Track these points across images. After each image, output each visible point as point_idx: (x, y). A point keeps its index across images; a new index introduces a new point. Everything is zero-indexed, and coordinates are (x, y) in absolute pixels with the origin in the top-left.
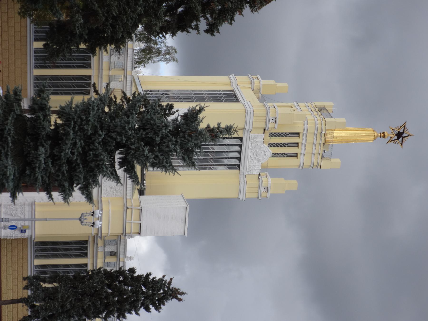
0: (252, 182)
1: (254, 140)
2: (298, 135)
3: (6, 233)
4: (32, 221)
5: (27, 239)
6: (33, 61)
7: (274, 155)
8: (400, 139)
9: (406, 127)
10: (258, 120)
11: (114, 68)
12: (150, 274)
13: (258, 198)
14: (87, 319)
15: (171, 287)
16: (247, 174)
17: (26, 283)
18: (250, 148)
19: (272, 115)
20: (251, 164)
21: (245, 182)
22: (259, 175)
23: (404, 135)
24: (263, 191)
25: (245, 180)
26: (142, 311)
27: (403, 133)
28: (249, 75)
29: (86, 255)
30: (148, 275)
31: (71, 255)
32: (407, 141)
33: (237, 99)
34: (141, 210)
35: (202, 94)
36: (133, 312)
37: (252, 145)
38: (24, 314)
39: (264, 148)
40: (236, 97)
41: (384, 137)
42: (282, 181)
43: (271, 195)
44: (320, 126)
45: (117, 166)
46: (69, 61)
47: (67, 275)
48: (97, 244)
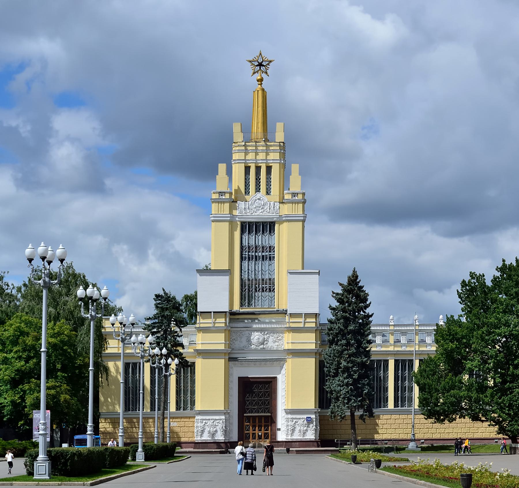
1: (243, 210)
2: (247, 169)
3: (221, 436)
8: (260, 61)
9: (251, 59)
10: (222, 209)
14: (371, 359)
16: (278, 215)
18: (252, 214)
20: (269, 211)
21: (285, 216)
24: (297, 198)
25: (284, 216)
32: (268, 56)
34: (290, 314)
36: (370, 319)
37: (249, 212)
39: (253, 200)
46: (159, 381)
47: (462, 361)
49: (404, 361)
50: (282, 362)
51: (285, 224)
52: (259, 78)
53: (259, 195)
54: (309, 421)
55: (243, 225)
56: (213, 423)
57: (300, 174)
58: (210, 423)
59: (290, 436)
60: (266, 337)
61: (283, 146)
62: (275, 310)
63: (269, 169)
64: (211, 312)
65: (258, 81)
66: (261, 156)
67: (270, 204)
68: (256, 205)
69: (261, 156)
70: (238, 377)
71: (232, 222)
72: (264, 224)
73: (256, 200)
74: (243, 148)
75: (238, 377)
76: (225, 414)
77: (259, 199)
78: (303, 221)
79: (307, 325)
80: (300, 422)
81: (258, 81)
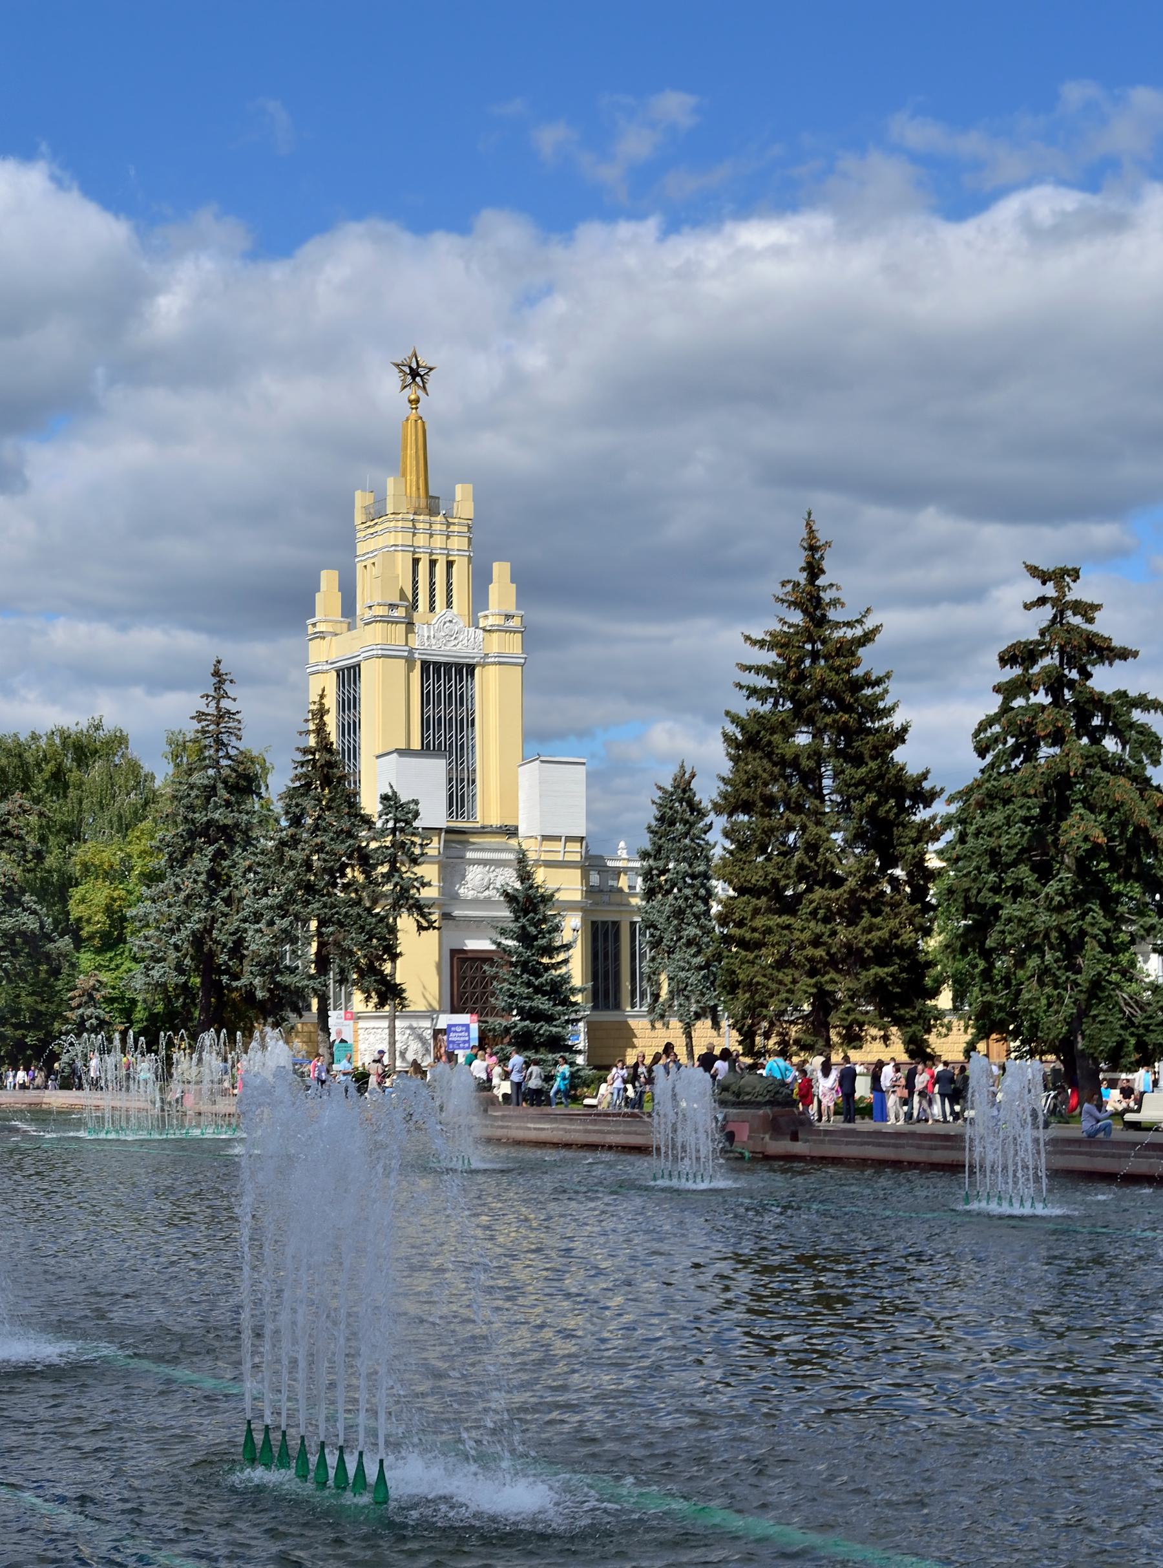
0: (495, 644)
7: (449, 604)
11: (102, 808)
13: (522, 665)
15: (671, 789)
17: (658, 1025)
19: (380, 611)
22: (485, 630)
23: (414, 366)
28: (470, 855)
29: (616, 925)
33: (354, 667)
35: (343, 725)
40: (349, 669)
41: (417, 401)
42: (493, 589)
43: (517, 608)
44: (400, 524)
45: (554, 961)
51: (492, 671)
52: (413, 397)
53: (450, 614)
55: (425, 665)
57: (512, 582)
59: (1028, 1204)
60: (492, 875)
62: (479, 825)
65: (410, 401)
66: (438, 541)
68: (447, 631)
69: (438, 541)
71: (410, 661)
72: (459, 667)
77: (451, 621)
79: (569, 857)
81: (410, 401)
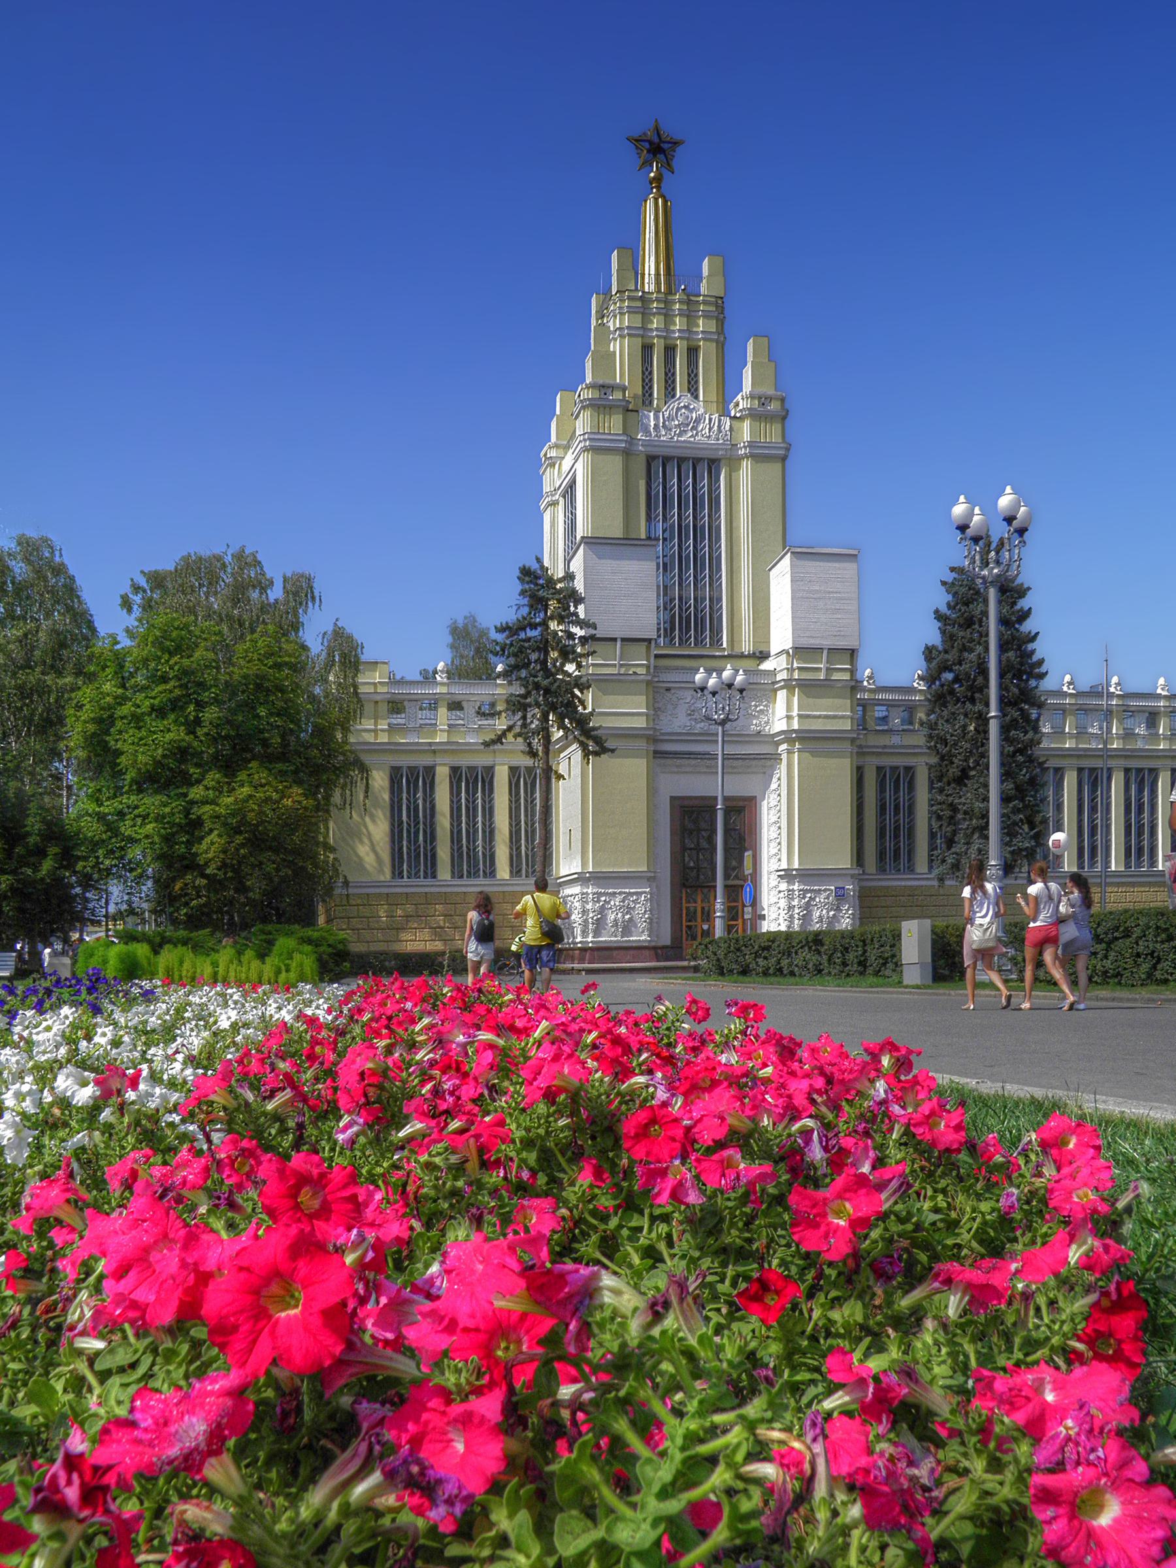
4: (1107, 884)
5: (861, 888)
6: (421, 881)
7: (693, 389)
12: (937, 612)
23: (656, 140)
26: (1028, 626)
27: (650, 142)
30: (938, 616)
31: (910, 799)
32: (671, 129)
36: (1030, 646)
38: (431, 1461)
48: (885, 747)
49: (413, 771)
50: (769, 763)
54: (840, 895)
56: (623, 901)
58: (617, 901)
61: (719, 307)
63: (692, 352)
64: (615, 640)
67: (710, 420)
70: (671, 797)
73: (678, 409)
74: (639, 304)
75: (671, 797)
76: (649, 879)
78: (784, 459)
80: (820, 899)
